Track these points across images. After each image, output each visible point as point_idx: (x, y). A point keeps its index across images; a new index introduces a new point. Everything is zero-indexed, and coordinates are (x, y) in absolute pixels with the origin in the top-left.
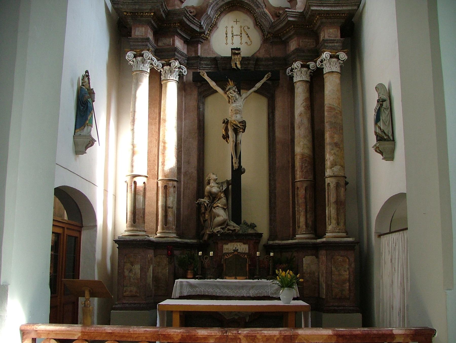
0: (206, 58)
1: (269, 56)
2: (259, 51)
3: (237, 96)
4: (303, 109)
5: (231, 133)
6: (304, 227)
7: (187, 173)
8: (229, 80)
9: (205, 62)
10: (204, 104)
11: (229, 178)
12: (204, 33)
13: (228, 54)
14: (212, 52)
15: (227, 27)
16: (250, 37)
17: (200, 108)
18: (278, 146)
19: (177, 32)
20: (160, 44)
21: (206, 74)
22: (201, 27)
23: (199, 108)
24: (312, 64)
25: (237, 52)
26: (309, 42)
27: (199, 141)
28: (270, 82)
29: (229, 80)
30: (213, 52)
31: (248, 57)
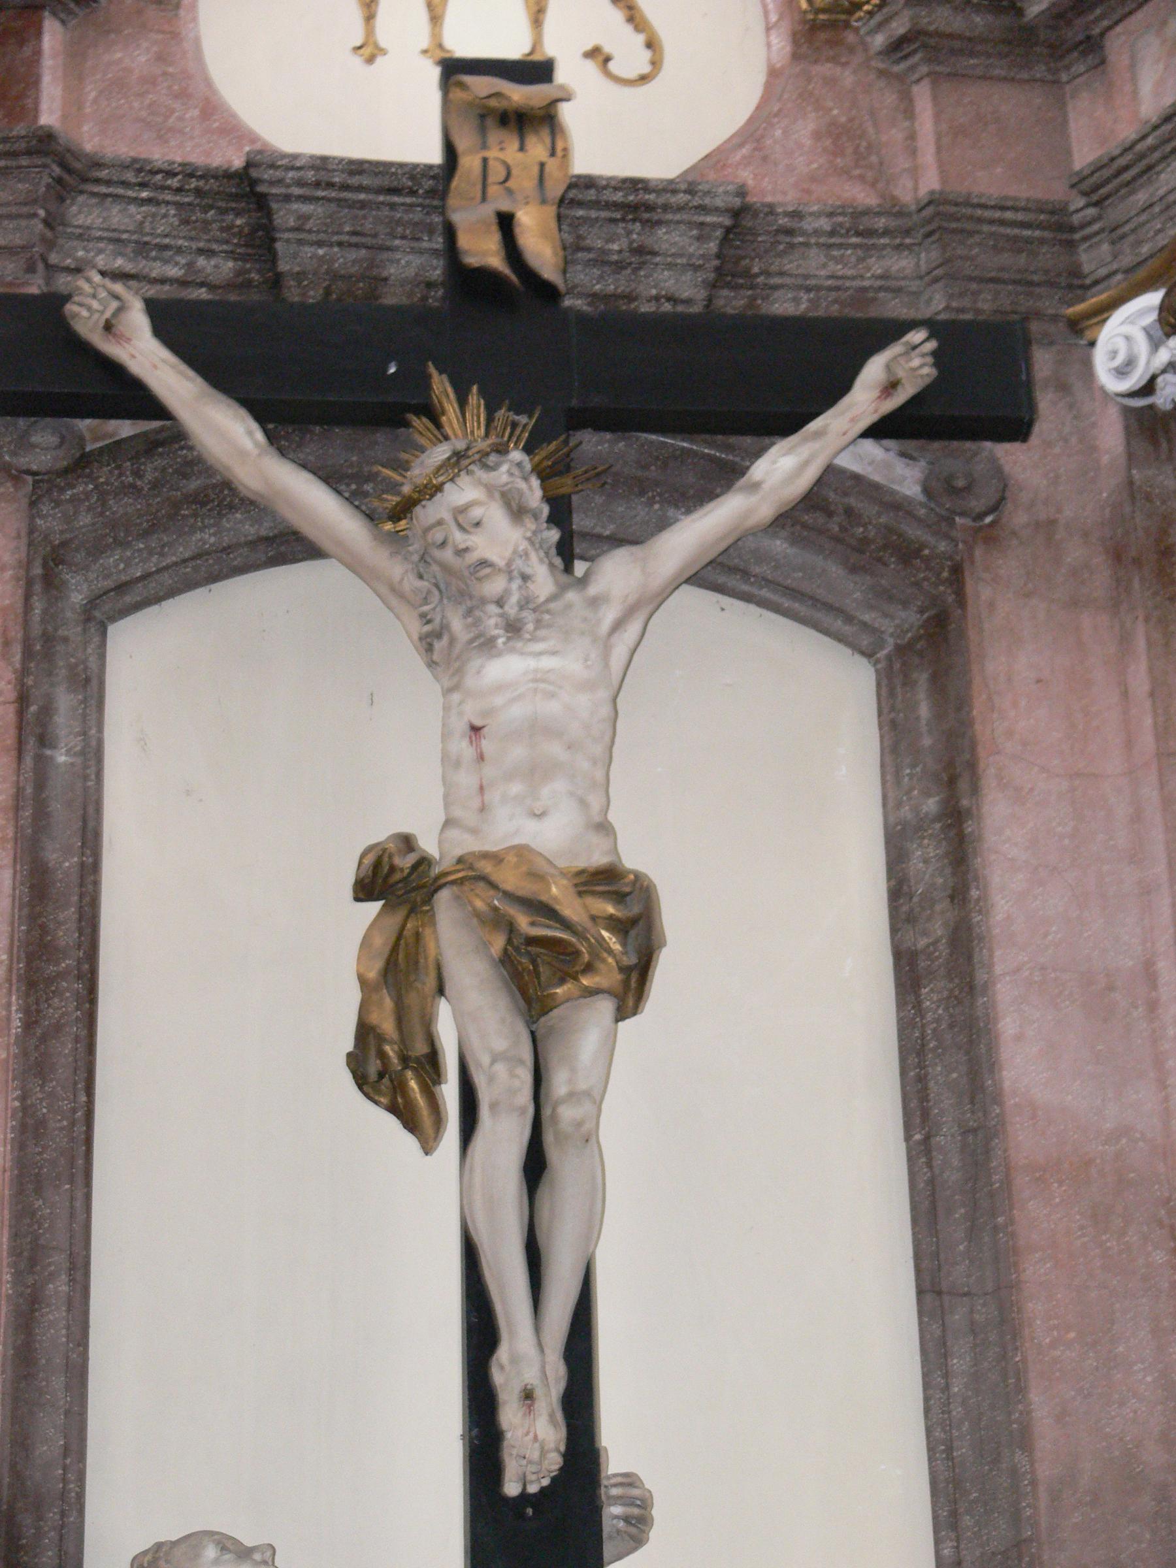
0: (145, 174)
1: (863, 196)
2: (753, 134)
3: (544, 581)
5: (470, 1019)
9: (121, 217)
10: (90, 686)
13: (404, 126)
17: (45, 740)
21: (138, 320)
25: (518, 94)
28: (899, 472)
30: (233, 129)
31: (635, 184)
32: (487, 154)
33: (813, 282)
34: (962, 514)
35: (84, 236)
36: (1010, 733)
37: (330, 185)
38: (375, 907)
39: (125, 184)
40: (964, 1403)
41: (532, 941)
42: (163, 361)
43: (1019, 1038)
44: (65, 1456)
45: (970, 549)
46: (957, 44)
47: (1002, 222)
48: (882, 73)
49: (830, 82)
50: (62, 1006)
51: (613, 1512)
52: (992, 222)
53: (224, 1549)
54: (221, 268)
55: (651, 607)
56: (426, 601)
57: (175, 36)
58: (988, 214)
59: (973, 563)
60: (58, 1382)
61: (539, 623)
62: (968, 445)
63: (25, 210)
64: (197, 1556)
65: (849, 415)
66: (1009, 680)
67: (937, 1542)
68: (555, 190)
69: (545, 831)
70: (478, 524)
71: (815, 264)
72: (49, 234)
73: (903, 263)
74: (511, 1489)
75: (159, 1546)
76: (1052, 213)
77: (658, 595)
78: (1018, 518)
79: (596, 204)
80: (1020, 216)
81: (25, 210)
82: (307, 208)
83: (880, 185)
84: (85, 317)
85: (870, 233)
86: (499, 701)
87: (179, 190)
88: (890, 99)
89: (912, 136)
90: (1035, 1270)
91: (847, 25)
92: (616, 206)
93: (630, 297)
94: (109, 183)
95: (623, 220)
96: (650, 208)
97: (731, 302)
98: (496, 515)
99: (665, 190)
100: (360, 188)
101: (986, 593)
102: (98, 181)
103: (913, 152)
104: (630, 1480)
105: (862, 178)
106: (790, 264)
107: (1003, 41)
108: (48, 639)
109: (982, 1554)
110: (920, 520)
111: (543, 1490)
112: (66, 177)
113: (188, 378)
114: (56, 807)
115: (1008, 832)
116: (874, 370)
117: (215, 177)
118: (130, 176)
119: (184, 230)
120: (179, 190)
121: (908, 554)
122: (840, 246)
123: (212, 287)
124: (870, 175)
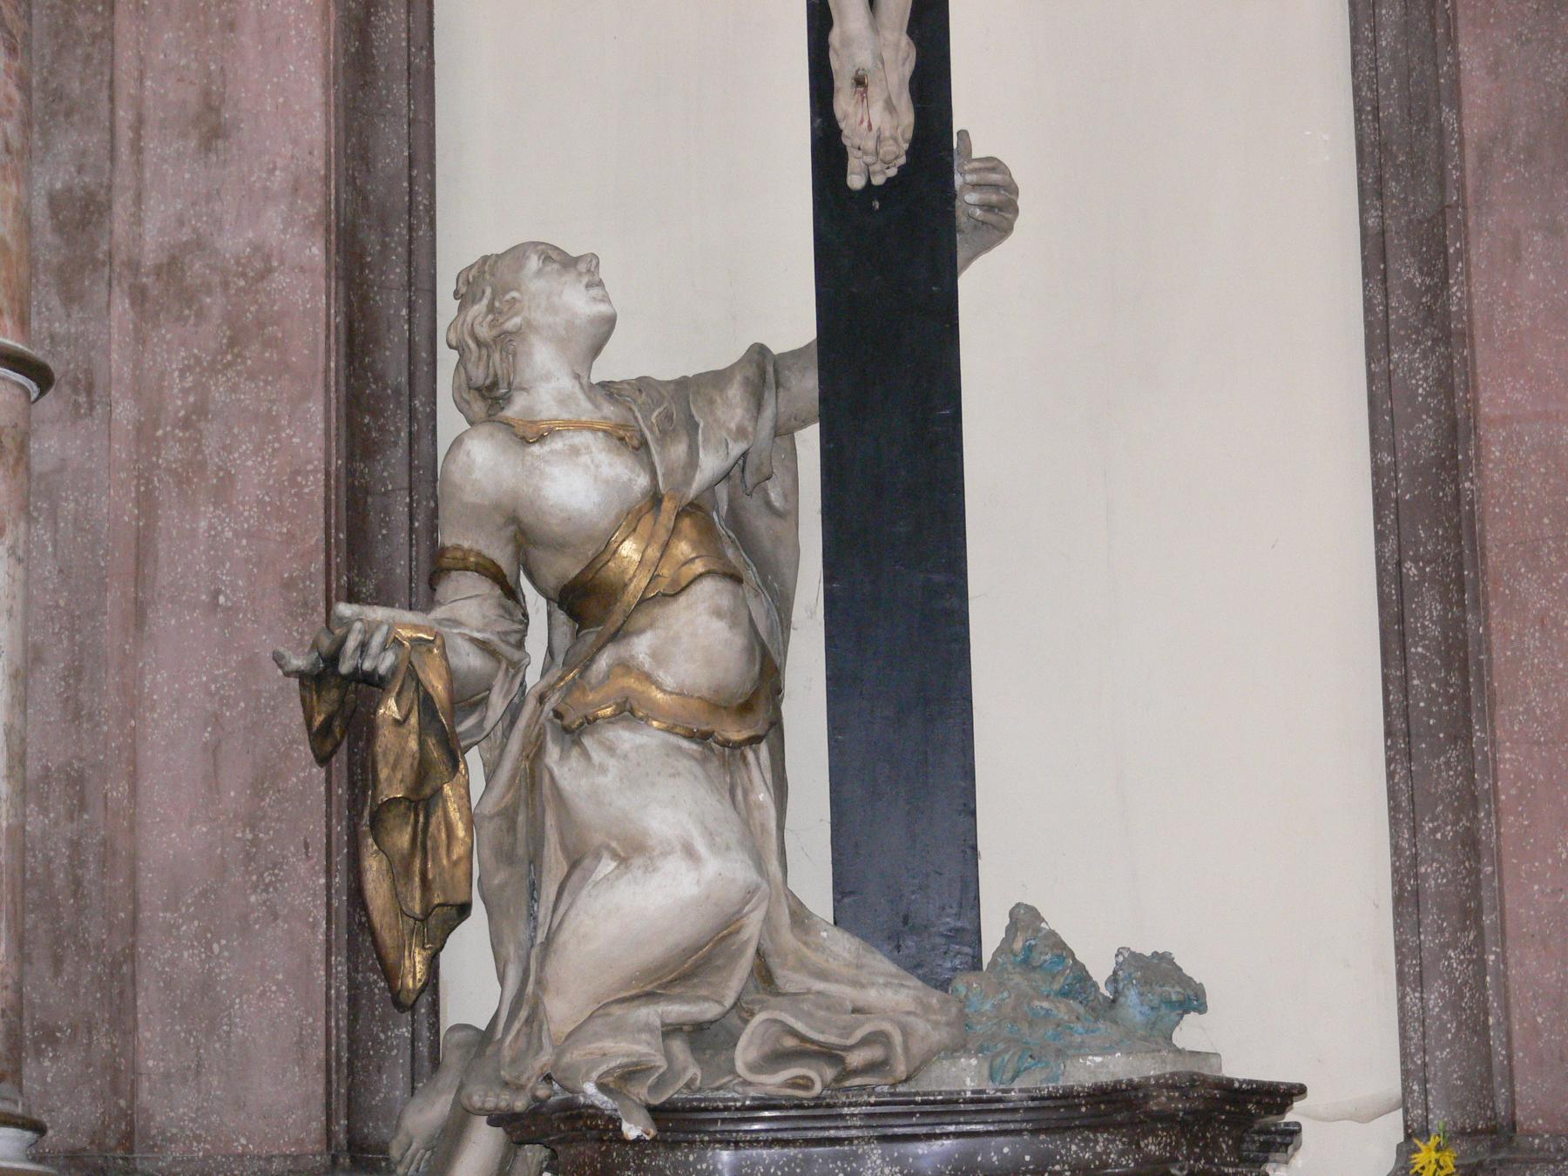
7: (196, 268)
11: (792, 322)
40: (1393, 59)
44: (410, 168)
51: (969, 199)
53: (548, 259)
60: (400, 89)
64: (521, 267)
67: (1363, 210)
74: (856, 181)
75: (485, 259)
104: (993, 165)
109: (1410, 221)
111: (889, 180)
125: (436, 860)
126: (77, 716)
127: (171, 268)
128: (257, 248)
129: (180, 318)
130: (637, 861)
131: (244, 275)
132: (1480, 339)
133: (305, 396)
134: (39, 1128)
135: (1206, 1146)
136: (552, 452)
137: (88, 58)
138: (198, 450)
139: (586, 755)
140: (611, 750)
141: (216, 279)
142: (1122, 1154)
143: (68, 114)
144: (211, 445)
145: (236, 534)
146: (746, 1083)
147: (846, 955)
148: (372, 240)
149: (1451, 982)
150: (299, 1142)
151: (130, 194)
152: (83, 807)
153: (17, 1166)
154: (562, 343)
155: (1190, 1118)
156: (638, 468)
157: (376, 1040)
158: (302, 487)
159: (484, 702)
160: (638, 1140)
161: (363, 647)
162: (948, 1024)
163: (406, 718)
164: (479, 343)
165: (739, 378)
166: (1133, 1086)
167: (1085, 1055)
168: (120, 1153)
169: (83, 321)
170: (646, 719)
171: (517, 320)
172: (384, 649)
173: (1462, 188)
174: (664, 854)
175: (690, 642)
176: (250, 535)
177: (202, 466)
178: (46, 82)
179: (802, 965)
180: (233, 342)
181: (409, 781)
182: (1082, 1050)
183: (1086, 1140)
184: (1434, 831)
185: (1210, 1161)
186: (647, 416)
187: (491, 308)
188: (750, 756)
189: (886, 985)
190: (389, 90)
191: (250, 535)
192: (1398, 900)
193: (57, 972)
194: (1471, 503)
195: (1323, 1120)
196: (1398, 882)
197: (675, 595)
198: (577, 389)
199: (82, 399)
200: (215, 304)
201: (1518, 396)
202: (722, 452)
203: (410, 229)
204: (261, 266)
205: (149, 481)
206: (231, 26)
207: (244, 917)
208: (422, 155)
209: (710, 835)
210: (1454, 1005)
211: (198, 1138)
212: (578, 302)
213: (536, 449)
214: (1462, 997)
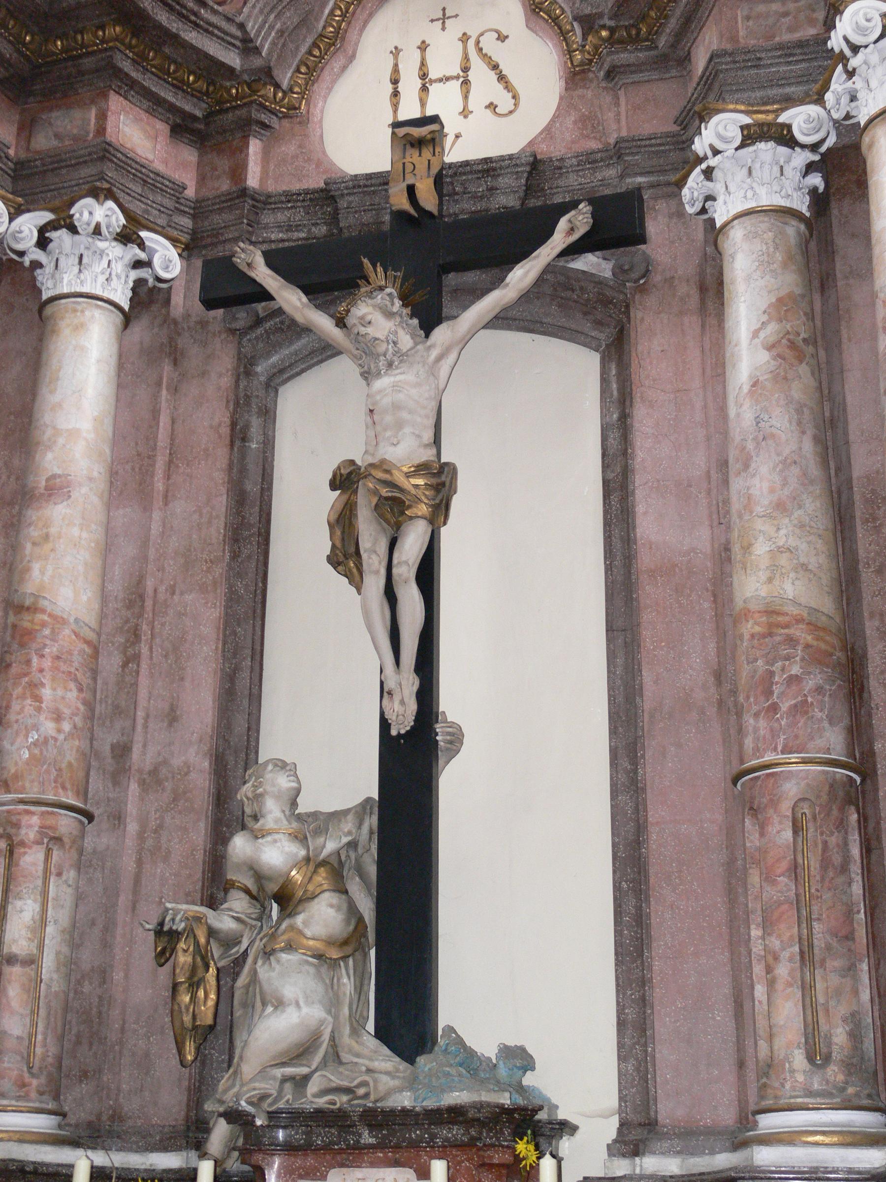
0: (290, 197)
1: (593, 145)
2: (548, 130)
4: (764, 357)
6: (799, 1059)
7: (164, 771)
8: (366, 261)
9: (281, 217)
10: (268, 414)
12: (267, 75)
14: (319, 164)
15: (396, 52)
16: (511, 78)
18: (650, 592)
19: (118, 73)
20: (43, 141)
22: (248, 47)
23: (238, 435)
24: (801, 119)
26: (786, 14)
27: (232, 598)
29: (366, 261)
31: (486, 160)
32: (405, 160)
33: (571, 188)
34: (628, 281)
35: (266, 227)
36: (648, 377)
37: (359, 186)
38: (339, 492)
39: (282, 202)
41: (387, 499)
42: (268, 275)
43: (645, 513)
45: (633, 297)
46: (633, 68)
47: (651, 146)
48: (604, 88)
49: (581, 97)
50: (249, 549)
52: (646, 146)
54: (321, 230)
55: (460, 346)
56: (361, 358)
57: (306, 136)
58: (643, 143)
59: (634, 302)
60: (246, 702)
61: (401, 362)
62: (632, 249)
63: (238, 221)
65: (551, 246)
66: (649, 353)
68: (435, 170)
69: (404, 451)
70: (370, 323)
71: (572, 180)
72: (251, 229)
73: (611, 172)
74: (394, 733)
76: (673, 136)
77: (461, 341)
78: (657, 278)
79: (471, 172)
80: (658, 141)
81: (238, 221)
82: (351, 198)
83: (603, 139)
84: (240, 260)
85: (595, 161)
86: (378, 398)
87: (304, 200)
88: (608, 99)
89: (618, 114)
90: (647, 617)
91: (589, 70)
92: (479, 171)
93: (487, 210)
94: (275, 203)
95: (483, 177)
96: (494, 169)
97: (533, 203)
98: (378, 318)
99: (499, 161)
100: (372, 185)
101: (639, 315)
102: (271, 203)
103: (619, 121)
105: (595, 138)
106: (561, 183)
107: (654, 63)
108: (247, 397)
110: (611, 287)
112: (256, 204)
113: (276, 280)
114: (251, 467)
115: (643, 420)
116: (563, 224)
117: (317, 192)
118: (283, 199)
119: (307, 217)
120: (304, 200)
121: (606, 302)
122: (582, 170)
123: (317, 238)
124: (598, 135)
125: (199, 1007)
126: (105, 946)
127: (154, 772)
128: (185, 763)
129: (157, 791)
130: (280, 1008)
131: (180, 774)
132: (649, 791)
133: (198, 820)
134: (64, 1115)
135: (497, 1132)
136: (267, 842)
137: (128, 692)
138: (159, 842)
139: (270, 964)
140: (278, 961)
141: (170, 775)
142: (463, 1135)
143: (120, 714)
144: (164, 840)
145: (170, 874)
146: (312, 1102)
147: (372, 1047)
148: (231, 759)
149: (637, 1059)
150: (176, 1120)
151: (140, 745)
152: (104, 983)
153: (54, 1131)
154: (278, 797)
155: (487, 1120)
156: (301, 848)
157: (212, 1077)
158: (194, 855)
159: (240, 942)
160: (262, 1125)
161: (173, 920)
162: (404, 1078)
163: (188, 949)
164: (248, 798)
165: (353, 811)
166: (462, 1107)
167: (452, 1091)
168: (108, 1123)
169: (119, 792)
170: (296, 950)
171: (261, 790)
172: (181, 921)
173: (643, 730)
174: (289, 1005)
175: (322, 917)
176: (175, 875)
177: (160, 848)
178: (113, 702)
179: (350, 1051)
180: (174, 800)
181: (187, 975)
182: (451, 1089)
183: (449, 1128)
184: (631, 995)
185: (498, 1139)
186: (309, 826)
187: (253, 786)
188: (342, 964)
189: (382, 1060)
190: (241, 701)
191: (175, 875)
192: (619, 1024)
193: (90, 1049)
194: (645, 858)
195: (588, 1117)
196: (618, 1017)
197: (313, 898)
198: (282, 816)
199: (117, 822)
200: (168, 785)
201: (663, 813)
202: (338, 841)
203: (247, 755)
204: (187, 769)
205: (141, 854)
206: (182, 679)
207: (163, 1027)
208: (254, 727)
209: (306, 997)
210: (637, 1069)
211: (139, 1117)
212: (284, 782)
213: (260, 840)
214: (640, 1065)
